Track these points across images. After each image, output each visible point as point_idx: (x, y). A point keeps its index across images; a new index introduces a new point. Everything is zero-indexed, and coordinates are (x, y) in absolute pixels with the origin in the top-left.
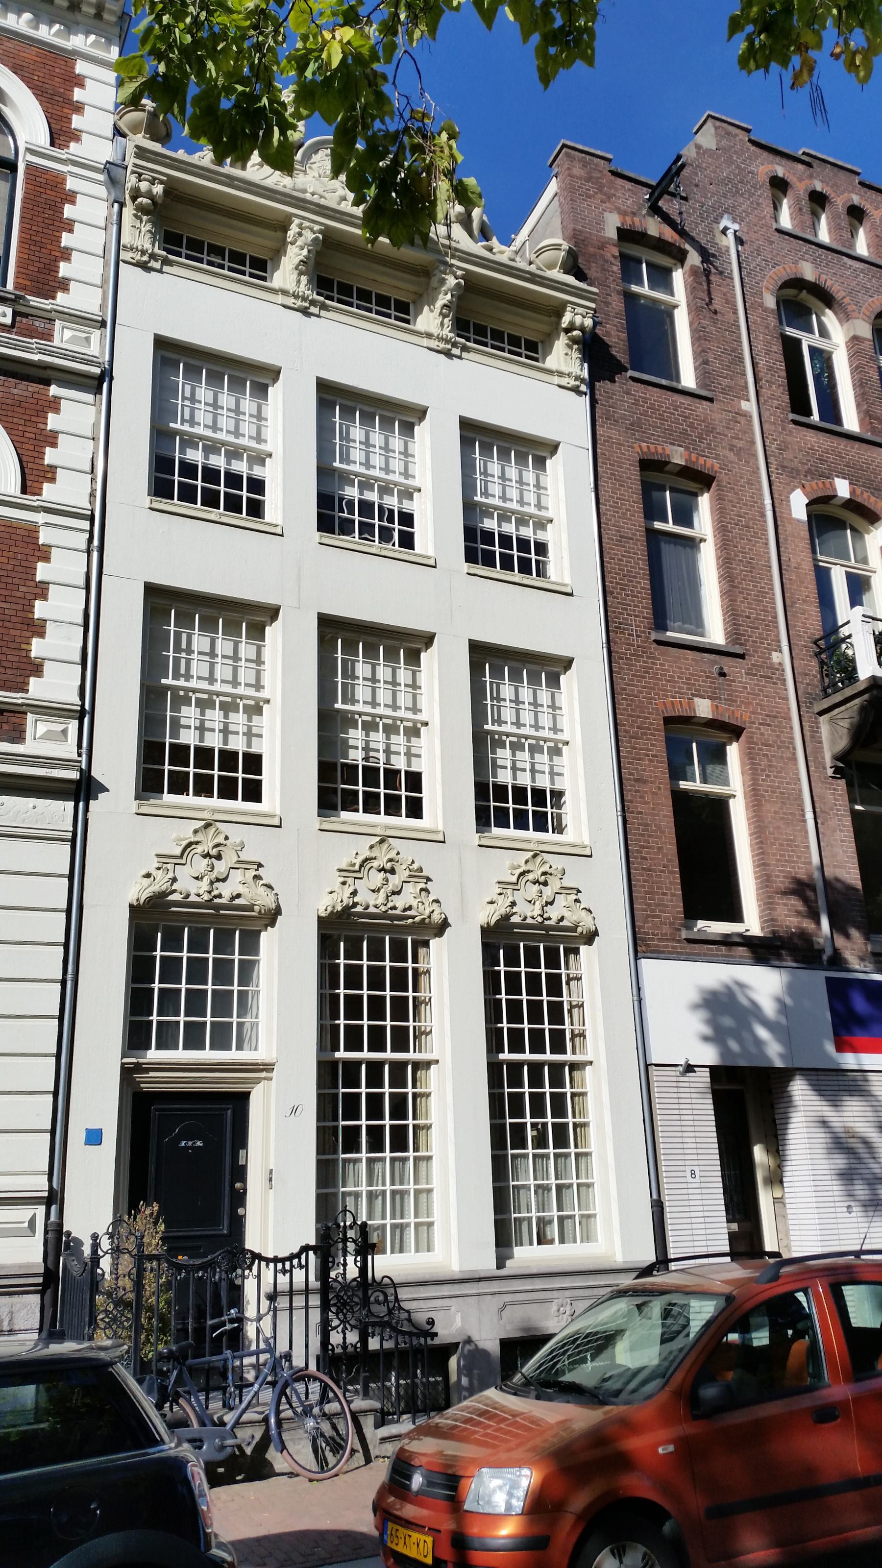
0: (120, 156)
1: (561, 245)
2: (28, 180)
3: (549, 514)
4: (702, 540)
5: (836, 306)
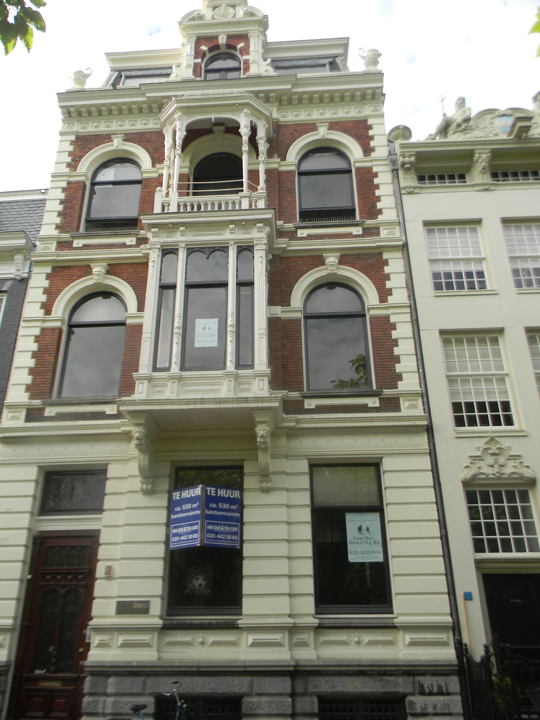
2: (356, 174)
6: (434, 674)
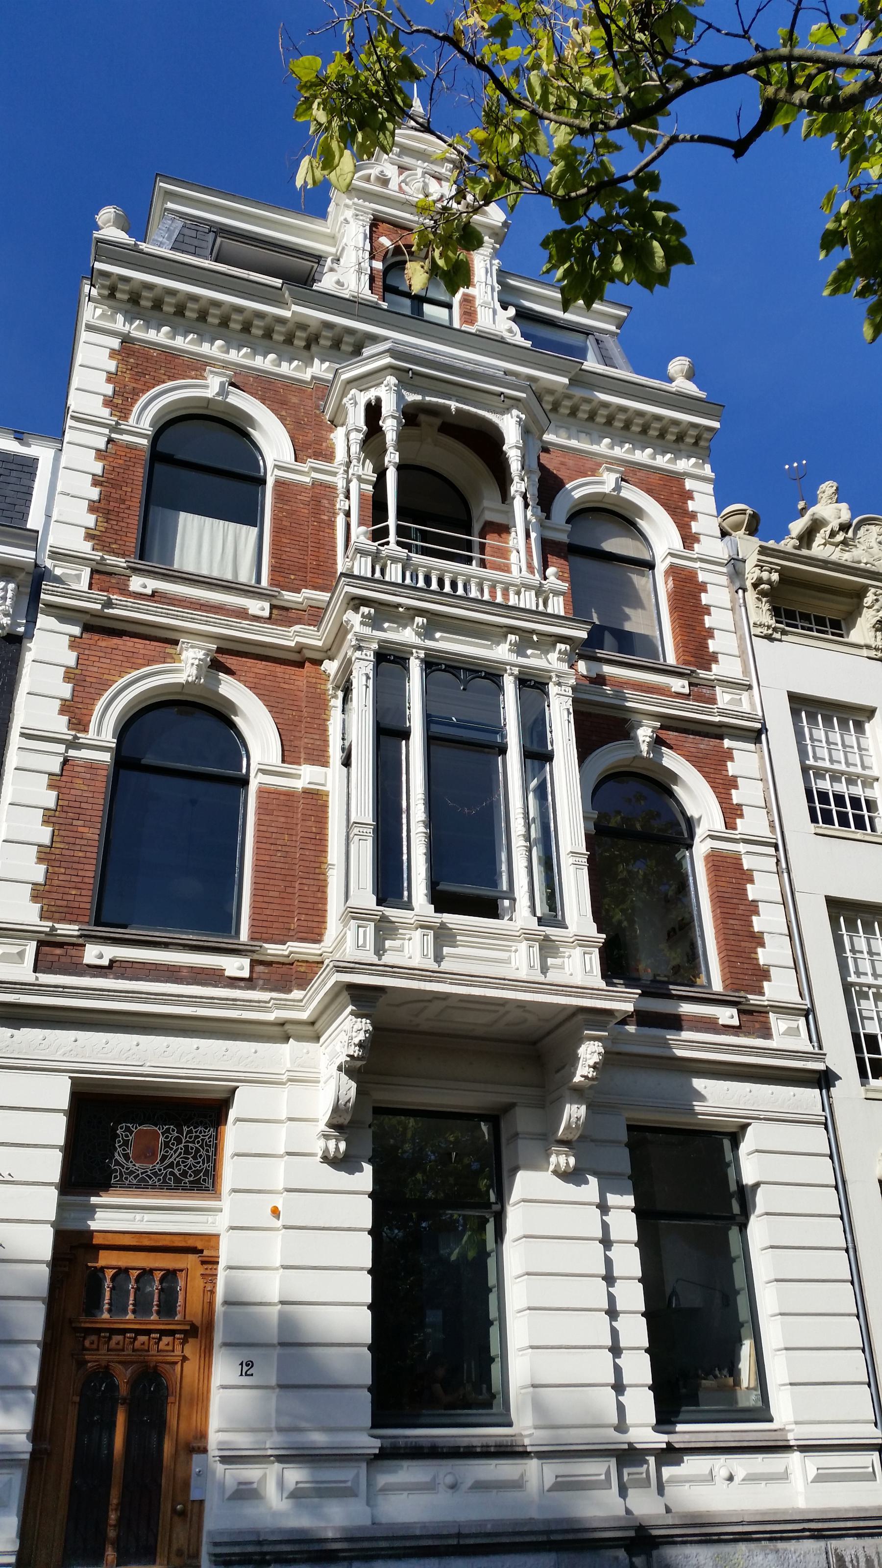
0: (736, 553)
1: (746, 510)
3: (875, 772)
6: (860, 1534)
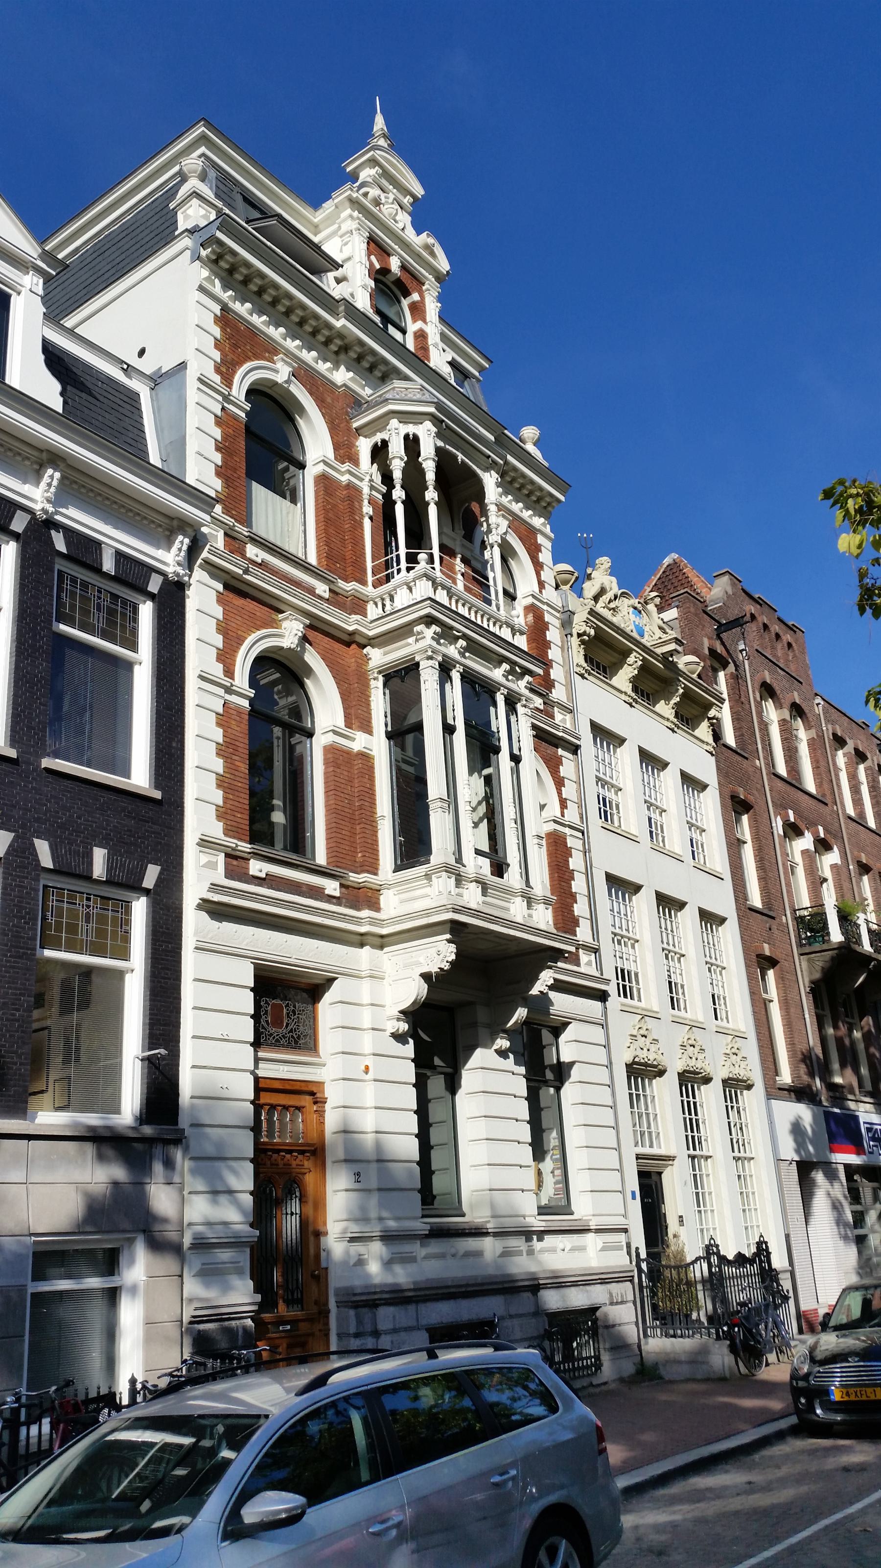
4: (745, 843)
5: (775, 699)
